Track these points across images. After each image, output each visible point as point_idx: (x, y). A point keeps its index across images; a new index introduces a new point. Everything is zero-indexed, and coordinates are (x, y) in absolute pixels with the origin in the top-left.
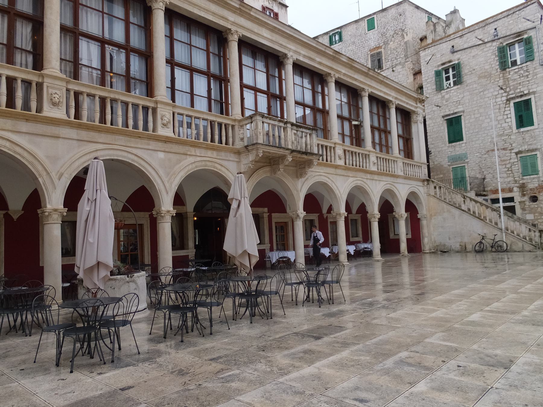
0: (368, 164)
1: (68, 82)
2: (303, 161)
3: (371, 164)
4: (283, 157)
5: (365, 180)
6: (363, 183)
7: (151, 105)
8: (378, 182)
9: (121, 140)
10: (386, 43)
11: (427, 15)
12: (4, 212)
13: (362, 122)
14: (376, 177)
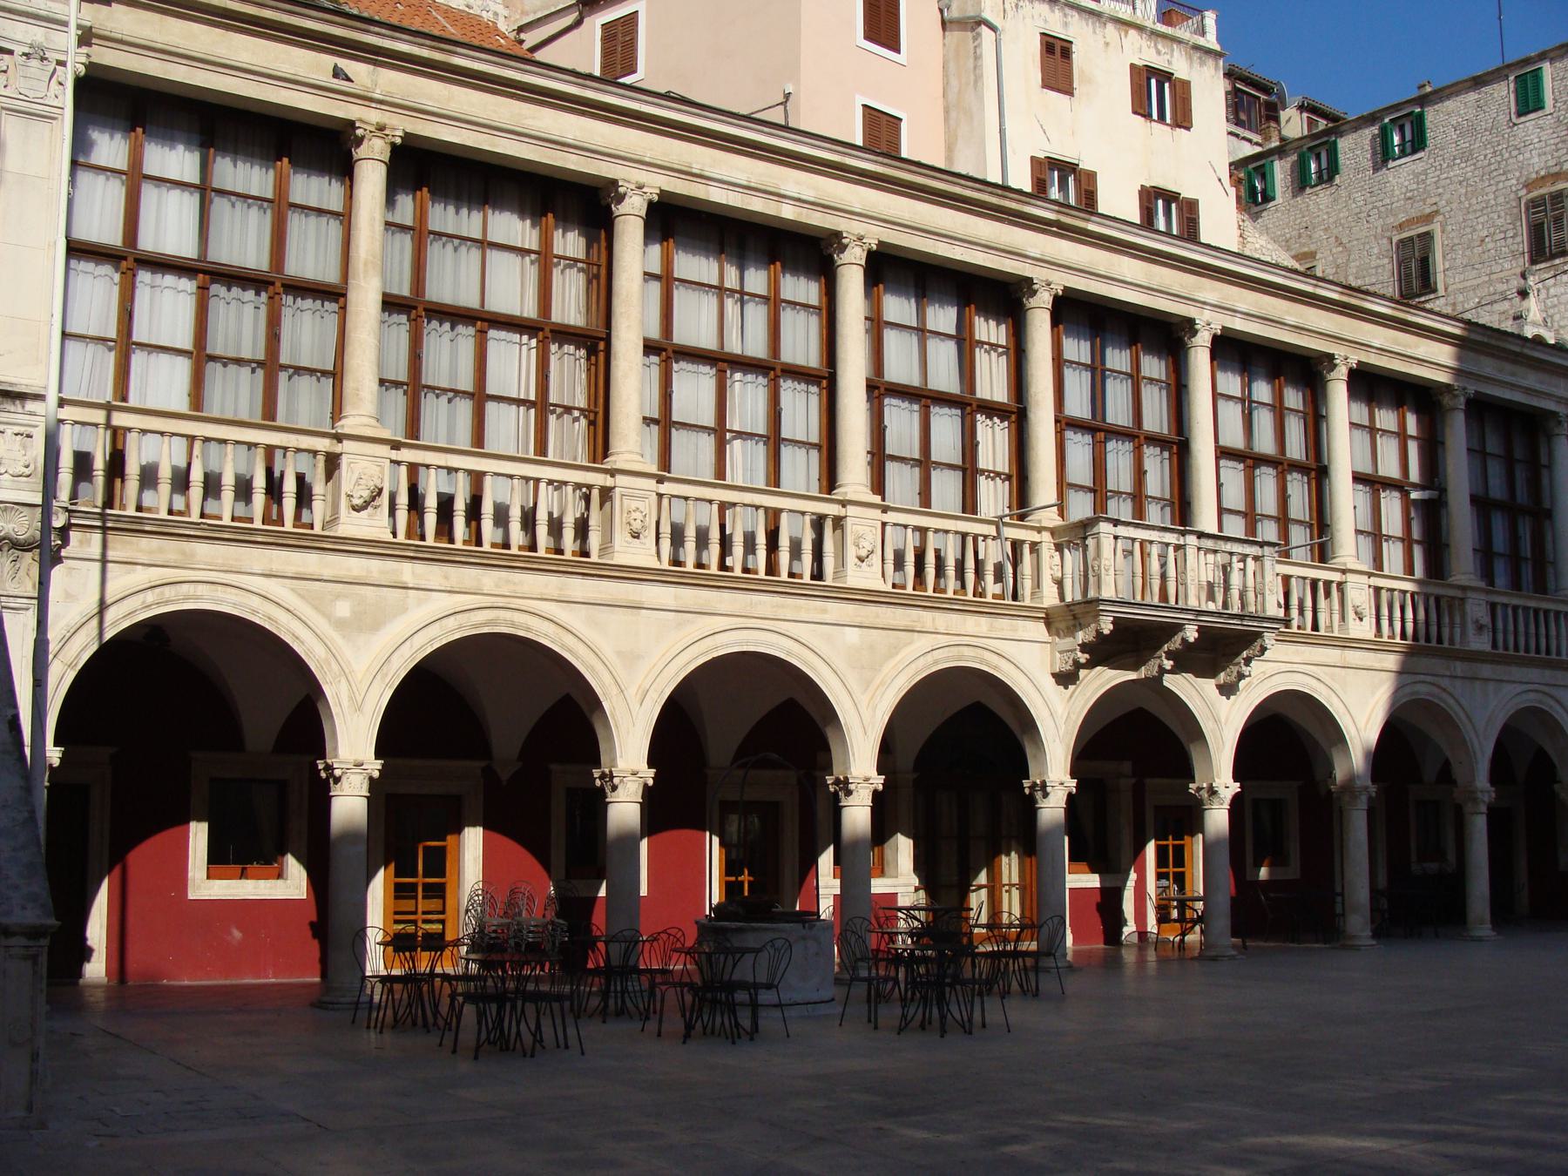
0: (1458, 631)
2: (1222, 649)
4: (1177, 628)
5: (1445, 683)
6: (1435, 690)
7: (832, 510)
8: (1491, 686)
9: (764, 603)
12: (483, 764)
13: (1443, 491)
14: (1486, 670)
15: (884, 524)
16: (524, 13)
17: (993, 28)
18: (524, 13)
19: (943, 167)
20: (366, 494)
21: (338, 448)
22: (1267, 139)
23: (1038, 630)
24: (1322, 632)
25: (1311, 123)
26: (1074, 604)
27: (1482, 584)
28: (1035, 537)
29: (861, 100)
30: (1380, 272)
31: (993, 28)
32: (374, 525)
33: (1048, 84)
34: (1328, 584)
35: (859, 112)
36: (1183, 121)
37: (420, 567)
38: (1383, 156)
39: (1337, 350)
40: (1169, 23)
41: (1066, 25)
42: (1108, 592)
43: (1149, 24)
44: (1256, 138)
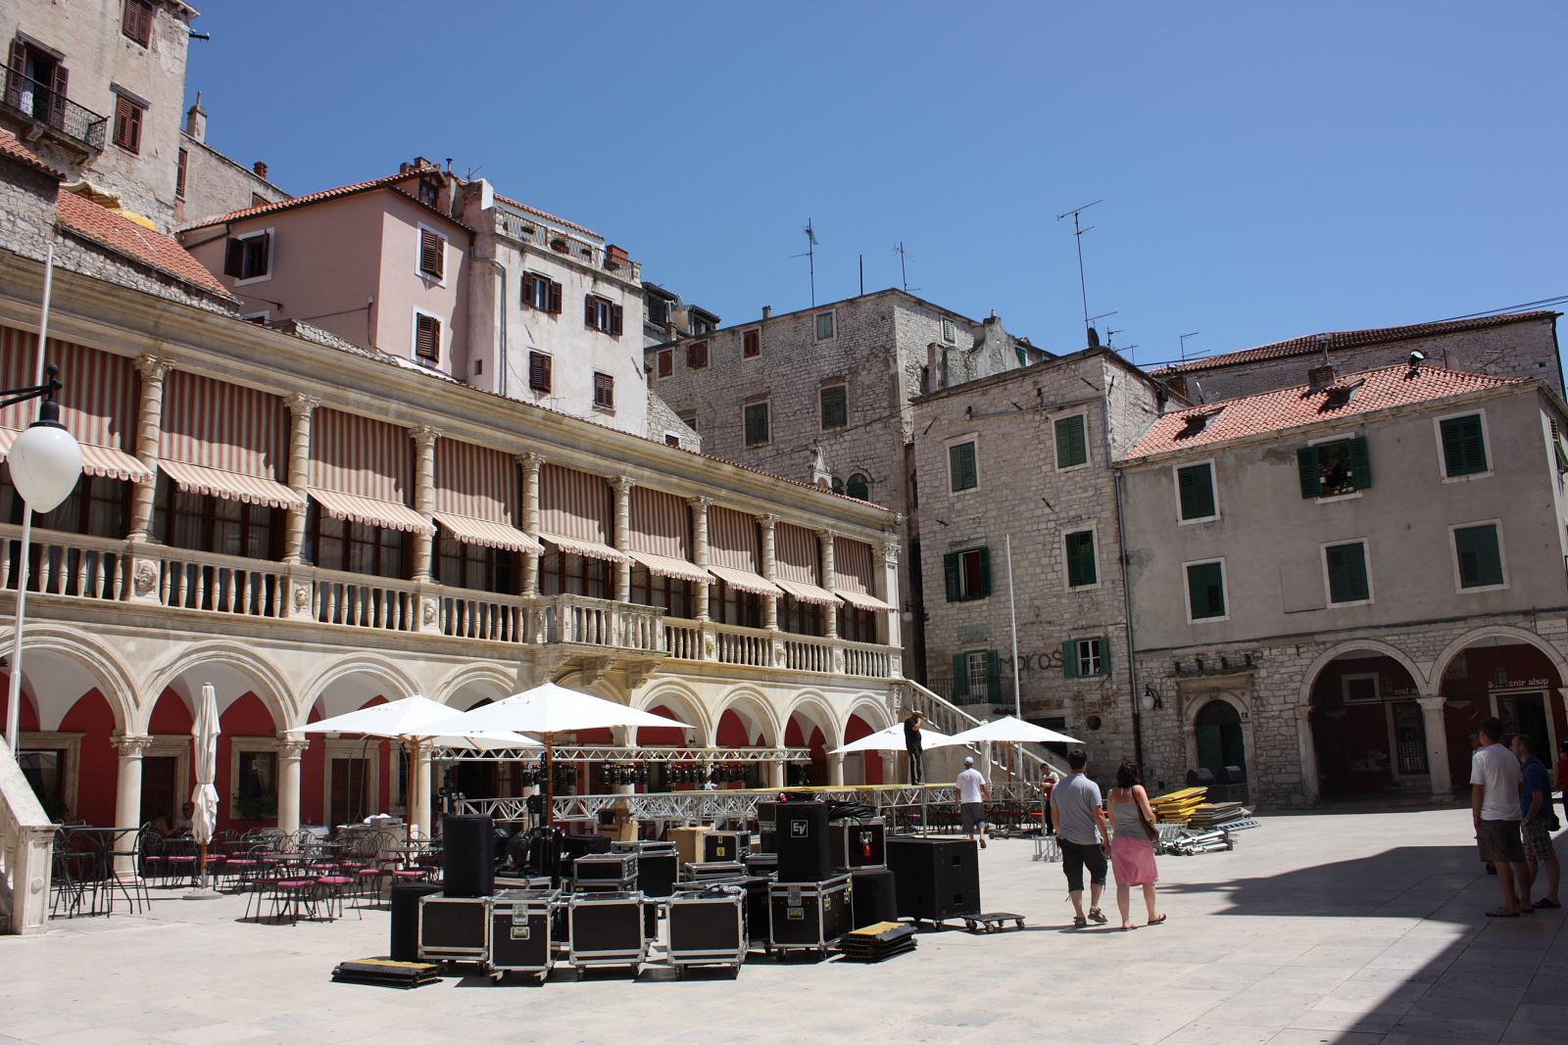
10: (854, 372)
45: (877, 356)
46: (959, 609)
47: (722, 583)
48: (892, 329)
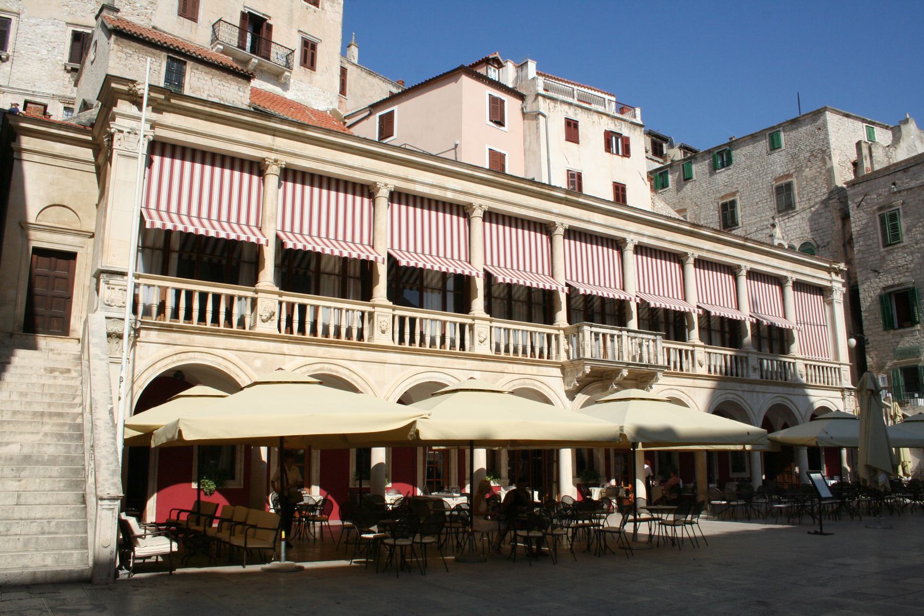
0: (745, 371)
1: (394, 310)
3: (751, 370)
5: (740, 393)
8: (761, 395)
9: (533, 370)
10: (799, 170)
11: (865, 124)
15: (491, 327)
16: (347, 111)
17: (544, 116)
18: (347, 111)
19: (521, 175)
20: (268, 315)
21: (256, 296)
22: (666, 161)
23: (557, 372)
24: (684, 372)
25: (685, 153)
26: (573, 360)
27: (755, 351)
28: (556, 332)
29: (488, 147)
30: (713, 217)
31: (544, 116)
32: (271, 328)
33: (568, 139)
34: (687, 351)
35: (487, 151)
36: (626, 153)
37: (291, 346)
38: (714, 168)
39: (689, 251)
40: (622, 113)
41: (576, 114)
42: (588, 356)
43: (611, 113)
44: (661, 160)
45: (816, 157)
46: (893, 335)
47: (707, 313)
48: (827, 134)
